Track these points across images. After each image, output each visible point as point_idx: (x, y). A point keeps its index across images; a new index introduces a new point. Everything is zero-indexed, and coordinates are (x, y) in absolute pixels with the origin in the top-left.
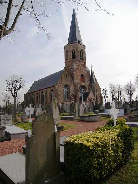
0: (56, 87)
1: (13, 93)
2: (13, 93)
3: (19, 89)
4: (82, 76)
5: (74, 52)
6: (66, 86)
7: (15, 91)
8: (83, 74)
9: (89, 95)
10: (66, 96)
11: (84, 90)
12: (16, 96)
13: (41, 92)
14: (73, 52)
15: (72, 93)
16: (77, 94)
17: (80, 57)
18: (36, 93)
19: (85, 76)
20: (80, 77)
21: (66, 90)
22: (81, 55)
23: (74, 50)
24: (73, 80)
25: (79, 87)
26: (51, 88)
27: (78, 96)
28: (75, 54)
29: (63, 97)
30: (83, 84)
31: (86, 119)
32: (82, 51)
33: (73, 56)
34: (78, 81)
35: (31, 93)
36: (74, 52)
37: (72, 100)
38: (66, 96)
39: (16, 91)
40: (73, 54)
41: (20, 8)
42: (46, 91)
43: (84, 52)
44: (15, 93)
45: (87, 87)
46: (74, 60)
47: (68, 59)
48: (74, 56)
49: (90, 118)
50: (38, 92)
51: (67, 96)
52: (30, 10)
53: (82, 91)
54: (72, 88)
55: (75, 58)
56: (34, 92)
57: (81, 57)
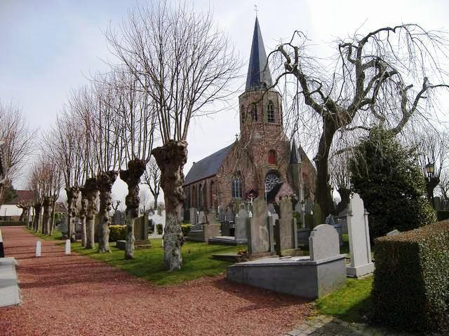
1: (153, 188)
2: (153, 188)
4: (273, 152)
7: (155, 184)
9: (281, 189)
10: (237, 192)
12: (158, 193)
13: (208, 185)
15: (249, 186)
16: (260, 188)
17: (266, 117)
18: (208, 181)
19: (278, 153)
20: (266, 156)
21: (238, 182)
22: (268, 112)
27: (260, 191)
29: (231, 195)
30: (273, 167)
34: (263, 163)
37: (250, 199)
38: (237, 192)
41: (362, 55)
42: (206, 183)
50: (195, 185)
51: (241, 189)
53: (272, 181)
54: (249, 176)
56: (189, 185)
57: (269, 116)
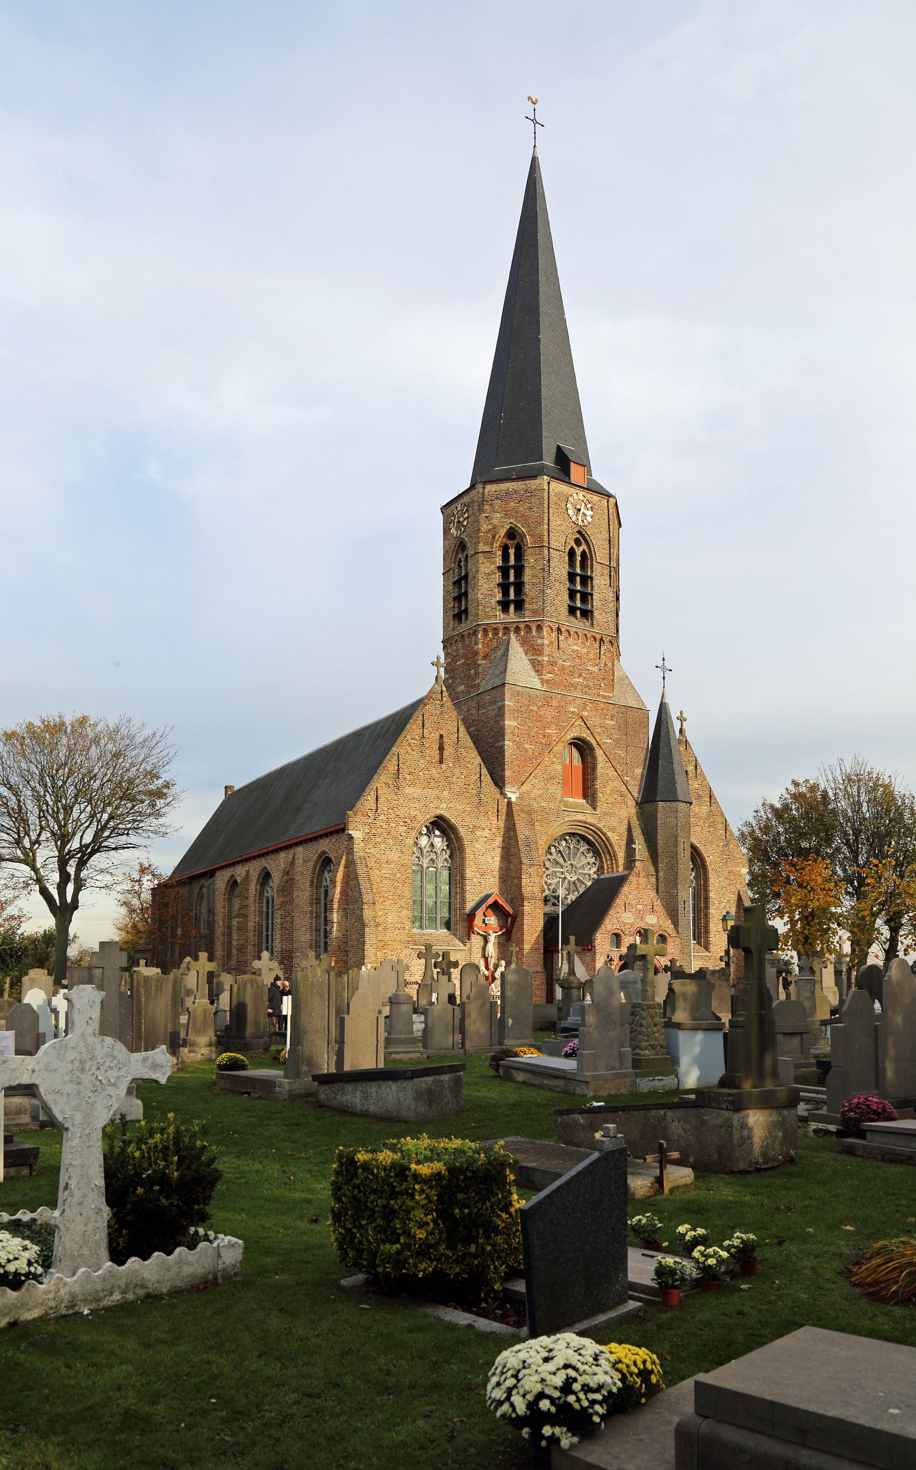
3: (96, 847)
5: (512, 551)
8: (585, 735)
9: (619, 901)
12: (75, 905)
13: (254, 876)
14: (505, 556)
24: (499, 782)
25: (543, 844)
26: (324, 845)
28: (519, 570)
31: (348, 1097)
32: (584, 547)
35: (193, 879)
36: (519, 555)
39: (73, 863)
43: (600, 554)
44: (65, 878)
45: (617, 840)
46: (512, 616)
47: (466, 611)
48: (513, 593)
49: (373, 1088)
50: (239, 872)
52: (610, 599)
55: (519, 605)
57: (572, 594)
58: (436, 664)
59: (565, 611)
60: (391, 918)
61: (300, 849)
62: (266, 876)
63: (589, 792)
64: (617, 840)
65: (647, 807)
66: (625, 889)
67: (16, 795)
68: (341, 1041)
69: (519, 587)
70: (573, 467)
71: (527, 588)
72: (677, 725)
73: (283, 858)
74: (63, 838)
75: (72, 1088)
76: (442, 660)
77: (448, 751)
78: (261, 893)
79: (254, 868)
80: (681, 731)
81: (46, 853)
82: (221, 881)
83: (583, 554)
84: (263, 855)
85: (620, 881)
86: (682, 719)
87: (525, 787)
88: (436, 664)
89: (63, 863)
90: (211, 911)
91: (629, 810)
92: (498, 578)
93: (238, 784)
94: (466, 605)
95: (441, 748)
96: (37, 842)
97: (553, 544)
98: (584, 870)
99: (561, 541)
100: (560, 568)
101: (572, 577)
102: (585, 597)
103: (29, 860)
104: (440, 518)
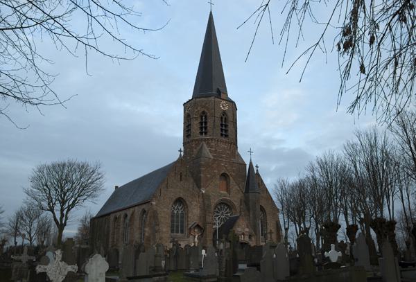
0: (152, 204)
5: (224, 119)
6: (180, 201)
11: (228, 210)
12: (65, 224)
19: (231, 178)
23: (204, 112)
26: (144, 206)
28: (206, 123)
33: (201, 128)
40: (201, 123)
43: (231, 119)
47: (190, 135)
50: (118, 214)
53: (222, 214)
55: (206, 133)
58: (180, 151)
59: (219, 135)
60: (164, 230)
61: (136, 208)
62: (126, 216)
63: (228, 190)
64: (237, 204)
65: (247, 194)
66: (238, 221)
67: (50, 190)
68: (135, 268)
69: (206, 128)
70: (222, 94)
71: (208, 128)
72: (255, 169)
73: (131, 210)
74: (63, 203)
75: (54, 273)
76: (182, 150)
77: (183, 177)
78: (124, 221)
79: (123, 213)
80: (257, 171)
81: (58, 207)
82: (112, 217)
83: (225, 119)
84: (126, 209)
85: (237, 218)
86: (257, 167)
87: (207, 189)
88: (180, 151)
89: (62, 210)
90: (108, 227)
91: (240, 195)
92: (199, 126)
93: (120, 185)
94: (66, 221)
95: (181, 176)
96: (55, 204)
97: (216, 115)
98: (225, 214)
99: (218, 115)
100: (218, 123)
101: (222, 125)
102: (226, 131)
103: (52, 210)
104: (183, 107)
